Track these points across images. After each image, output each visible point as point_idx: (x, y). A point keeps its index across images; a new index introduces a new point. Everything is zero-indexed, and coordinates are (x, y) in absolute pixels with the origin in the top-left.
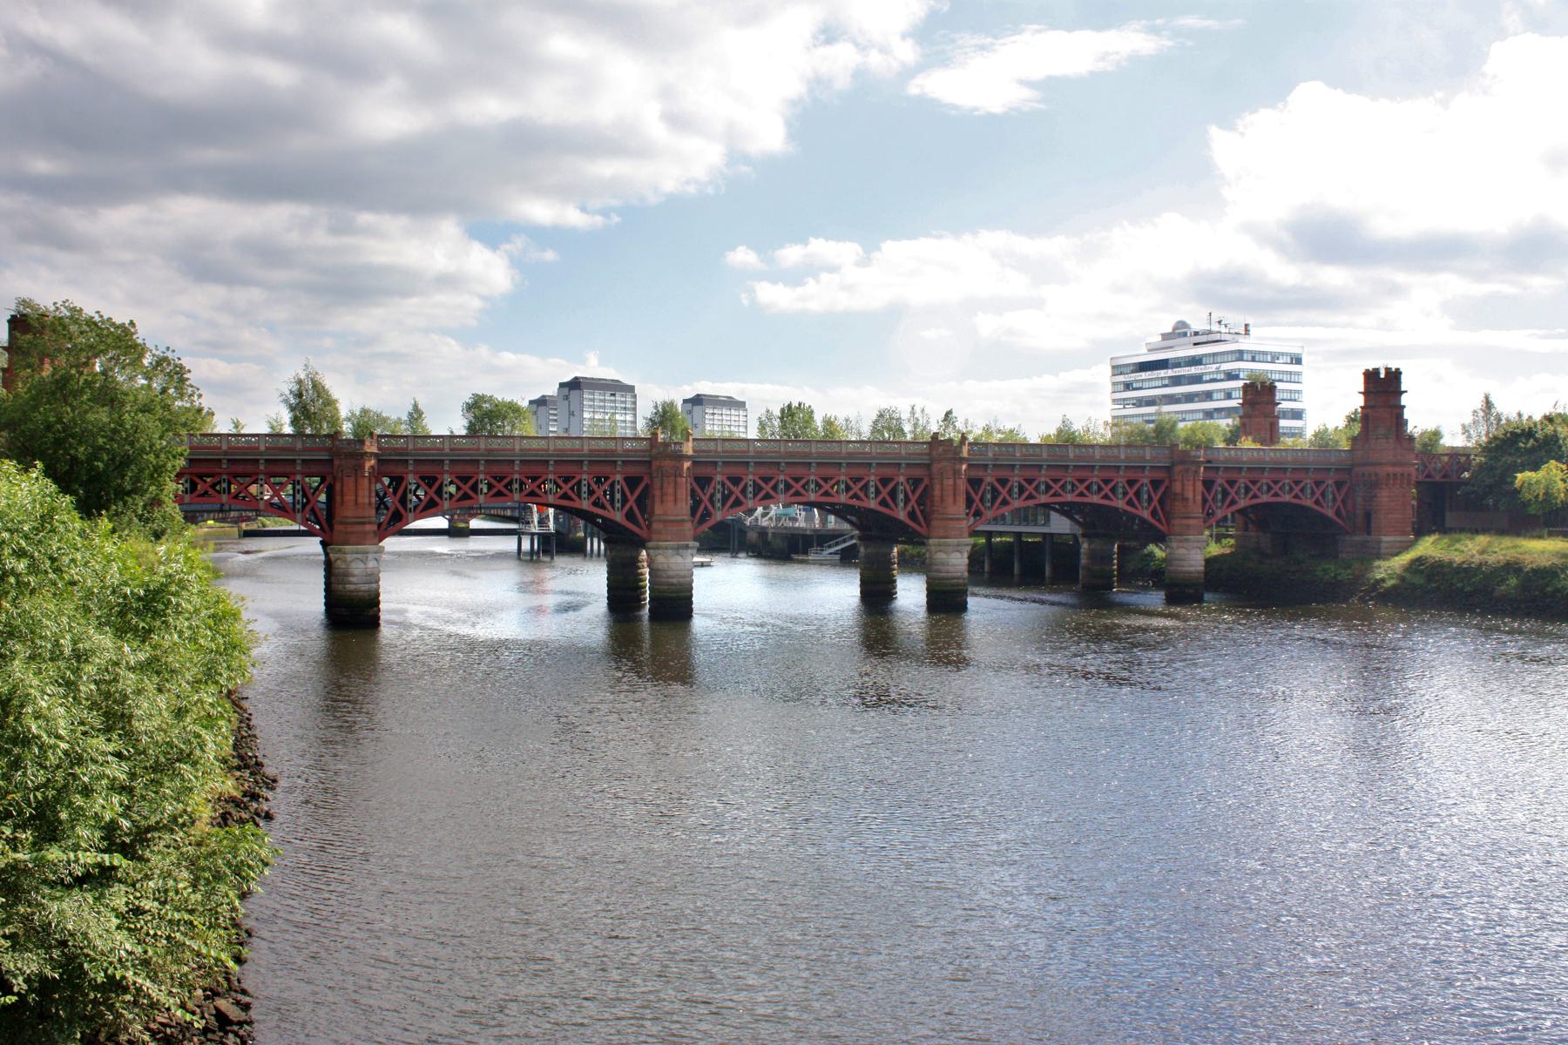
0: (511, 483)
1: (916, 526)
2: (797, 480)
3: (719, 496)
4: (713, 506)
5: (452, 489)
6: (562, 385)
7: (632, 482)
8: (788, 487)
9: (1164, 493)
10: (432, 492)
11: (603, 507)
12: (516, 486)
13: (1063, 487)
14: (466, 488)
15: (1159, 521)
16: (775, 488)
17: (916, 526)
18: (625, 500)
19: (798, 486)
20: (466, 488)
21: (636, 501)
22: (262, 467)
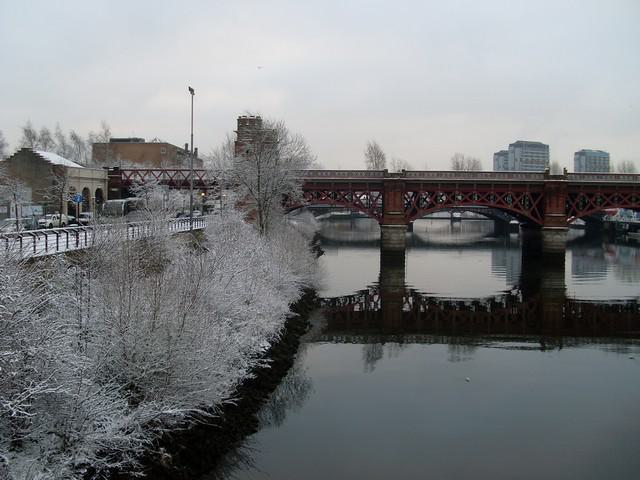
0: (489, 196)
1: (535, 220)
2: (625, 195)
3: (581, 204)
4: (578, 208)
5: (460, 198)
6: (511, 145)
7: (535, 196)
8: (620, 199)
9: (541, 201)
10: (449, 198)
11: (519, 209)
12: (492, 197)
13: (630, 200)
14: (467, 197)
15: (536, 216)
16: (612, 200)
17: (535, 220)
18: (530, 205)
19: (625, 199)
20: (467, 197)
21: (537, 206)
22: (350, 187)
